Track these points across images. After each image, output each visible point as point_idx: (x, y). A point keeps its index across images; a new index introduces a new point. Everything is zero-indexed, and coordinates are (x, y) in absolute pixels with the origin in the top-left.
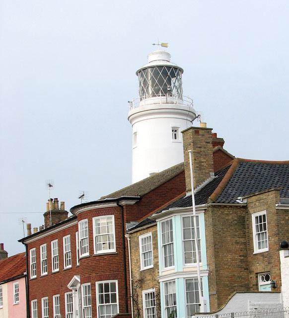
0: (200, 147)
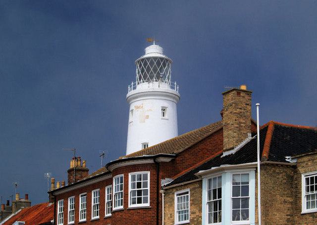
0: (240, 109)
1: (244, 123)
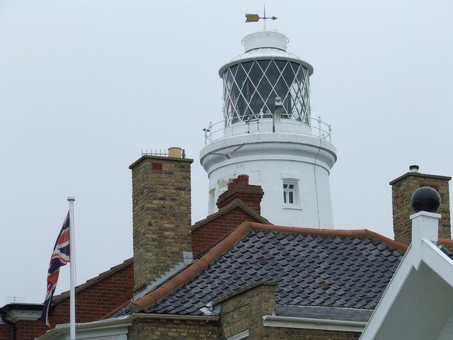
0: (161, 199)
1: (173, 230)
